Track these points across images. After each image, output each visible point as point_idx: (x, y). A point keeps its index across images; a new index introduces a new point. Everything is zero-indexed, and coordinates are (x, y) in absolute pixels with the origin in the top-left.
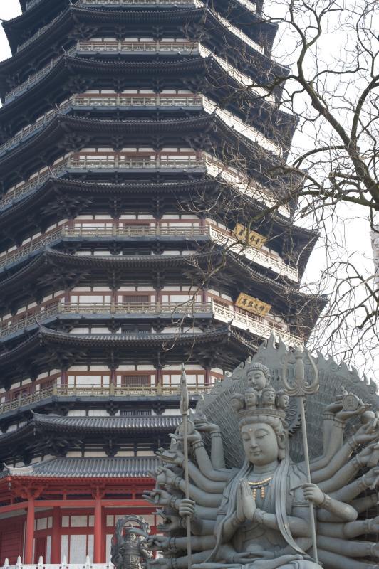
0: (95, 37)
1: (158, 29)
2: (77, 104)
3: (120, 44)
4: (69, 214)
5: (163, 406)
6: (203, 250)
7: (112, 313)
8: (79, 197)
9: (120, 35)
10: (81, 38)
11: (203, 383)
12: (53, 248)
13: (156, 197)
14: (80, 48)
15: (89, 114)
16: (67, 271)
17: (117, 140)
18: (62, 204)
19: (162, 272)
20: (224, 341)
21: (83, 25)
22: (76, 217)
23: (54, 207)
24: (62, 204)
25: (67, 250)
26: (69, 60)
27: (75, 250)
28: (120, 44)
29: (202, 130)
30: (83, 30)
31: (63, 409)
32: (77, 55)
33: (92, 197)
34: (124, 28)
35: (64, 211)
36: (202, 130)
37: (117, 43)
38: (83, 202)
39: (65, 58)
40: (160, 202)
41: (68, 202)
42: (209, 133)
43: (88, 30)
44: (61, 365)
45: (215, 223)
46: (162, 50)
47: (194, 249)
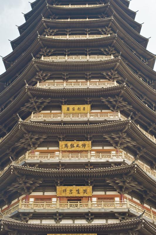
0: (43, 109)
1: (88, 74)
2: (23, 208)
3: (65, 83)
4: (26, 191)
5: (93, 217)
6: (123, 218)
7: (59, 159)
8: (33, 179)
9: (65, 78)
10: (41, 80)
11: (119, 200)
12: (12, 217)
13: (87, 135)
14: (34, 118)
15: (37, 165)
16: (27, 181)
17: (65, 74)
18: (21, 184)
19: (92, 181)
20: (132, 171)
21: (49, 29)
22: (31, 193)
23: (16, 186)
24: (21, 184)
25: (22, 219)
26: (15, 168)
27: (28, 219)
28: (65, 83)
29: (113, 68)
30: (42, 75)
31: (25, 219)
32: (25, 164)
33: (42, 179)
34: (68, 73)
35: (23, 189)
36: (113, 68)
37: (63, 83)
38: (36, 182)
39: (12, 167)
40: (91, 182)
41: (25, 183)
42: (125, 132)
43: (48, 51)
44: (26, 191)
45: (130, 197)
46: (92, 117)
47: (117, 218)
